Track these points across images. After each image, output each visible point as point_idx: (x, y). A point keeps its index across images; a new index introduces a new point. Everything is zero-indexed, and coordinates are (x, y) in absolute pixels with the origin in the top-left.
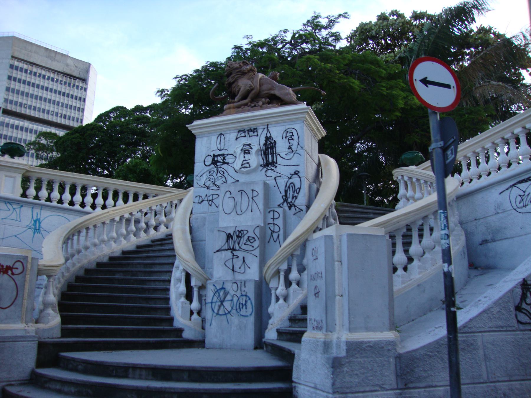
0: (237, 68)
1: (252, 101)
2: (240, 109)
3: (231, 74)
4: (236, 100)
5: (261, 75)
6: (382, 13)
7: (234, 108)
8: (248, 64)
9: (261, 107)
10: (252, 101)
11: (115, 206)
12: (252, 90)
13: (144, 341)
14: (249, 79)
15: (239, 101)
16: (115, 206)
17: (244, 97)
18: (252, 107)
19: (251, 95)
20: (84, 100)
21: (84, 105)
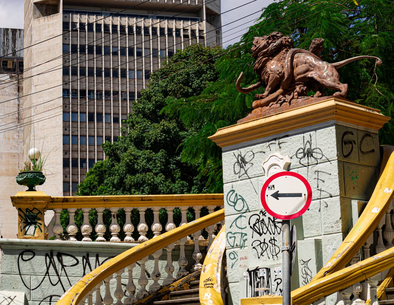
15: (267, 96)
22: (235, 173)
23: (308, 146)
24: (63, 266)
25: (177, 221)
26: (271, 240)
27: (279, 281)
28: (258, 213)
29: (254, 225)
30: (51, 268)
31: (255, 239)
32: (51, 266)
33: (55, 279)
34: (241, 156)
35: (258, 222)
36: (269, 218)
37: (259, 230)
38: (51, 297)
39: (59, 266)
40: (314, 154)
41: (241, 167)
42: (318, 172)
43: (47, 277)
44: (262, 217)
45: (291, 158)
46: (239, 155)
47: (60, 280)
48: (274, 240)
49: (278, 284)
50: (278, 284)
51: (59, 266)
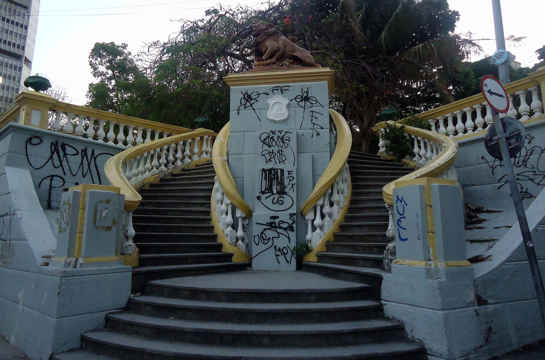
0: (264, 30)
1: (278, 59)
2: (270, 67)
3: (259, 34)
4: (264, 57)
5: (284, 37)
6: (456, 13)
7: (263, 65)
8: (273, 27)
9: (288, 67)
10: (278, 59)
11: (144, 143)
12: (278, 51)
13: (205, 266)
14: (275, 41)
15: (266, 60)
16: (144, 143)
17: (271, 57)
18: (281, 66)
19: (276, 55)
20: (26, 28)
21: (27, 33)
22: (42, 141)
23: (305, 95)
24: (65, 155)
25: (161, 136)
26: (279, 151)
27: (291, 178)
28: (269, 132)
29: (265, 140)
30: (55, 155)
31: (264, 149)
32: (55, 153)
33: (57, 163)
34: (247, 94)
35: (268, 138)
36: (278, 136)
37: (269, 143)
38: (53, 176)
39: (61, 154)
40: (310, 101)
41: (247, 101)
42: (313, 112)
43: (51, 160)
44: (271, 135)
45: (291, 100)
46: (245, 93)
47: (61, 165)
48: (281, 151)
49: (290, 181)
50: (290, 181)
51: (61, 154)
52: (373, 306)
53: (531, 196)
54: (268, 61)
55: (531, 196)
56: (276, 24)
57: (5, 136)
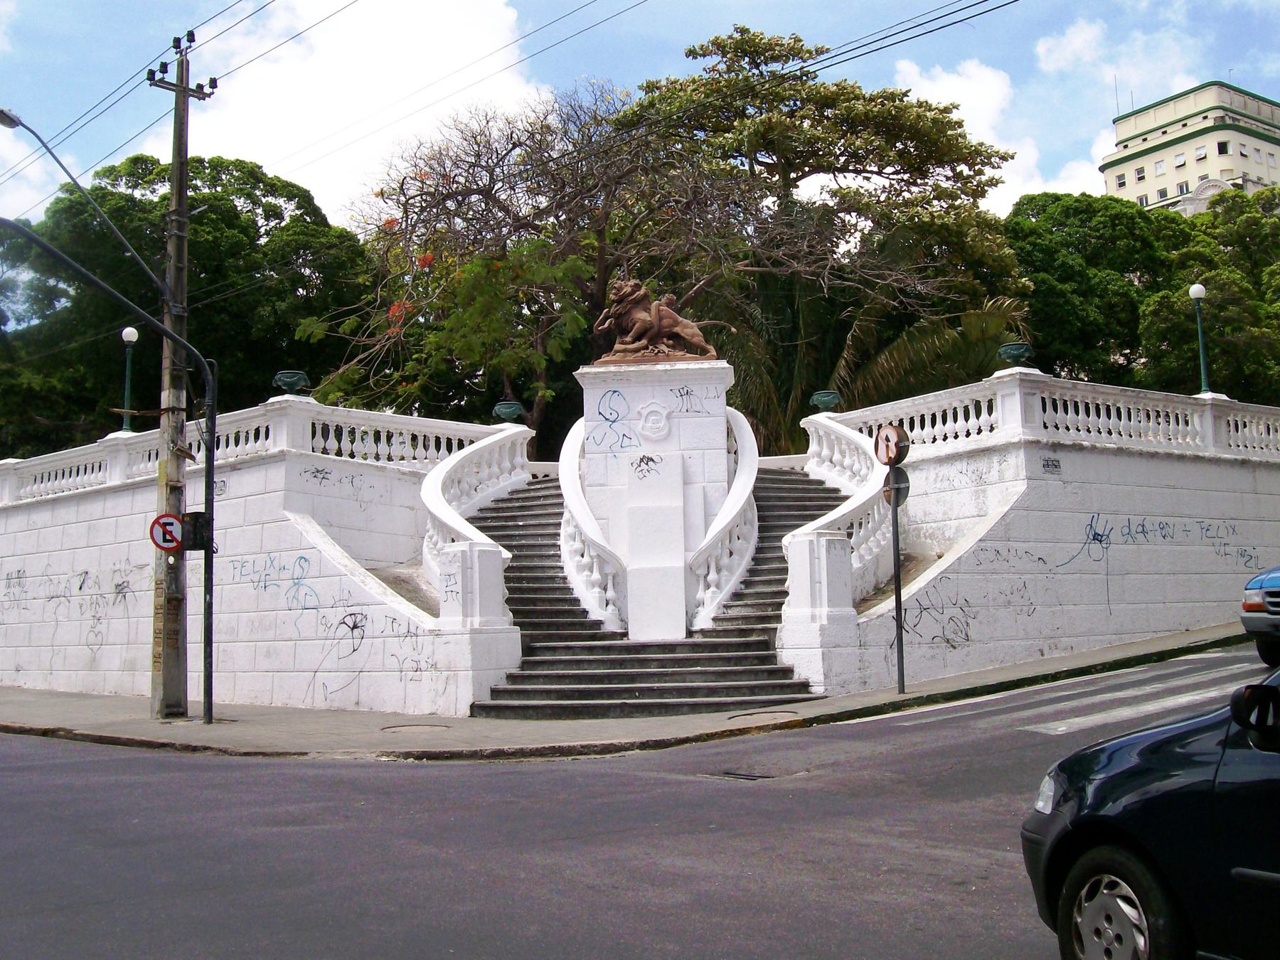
15: (633, 342)
52: (1153, 781)
53: (381, 194)
54: (637, 345)
55: (381, 194)
56: (573, 247)
57: (344, 765)
